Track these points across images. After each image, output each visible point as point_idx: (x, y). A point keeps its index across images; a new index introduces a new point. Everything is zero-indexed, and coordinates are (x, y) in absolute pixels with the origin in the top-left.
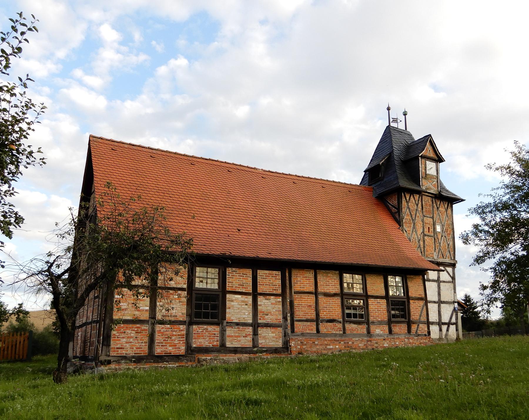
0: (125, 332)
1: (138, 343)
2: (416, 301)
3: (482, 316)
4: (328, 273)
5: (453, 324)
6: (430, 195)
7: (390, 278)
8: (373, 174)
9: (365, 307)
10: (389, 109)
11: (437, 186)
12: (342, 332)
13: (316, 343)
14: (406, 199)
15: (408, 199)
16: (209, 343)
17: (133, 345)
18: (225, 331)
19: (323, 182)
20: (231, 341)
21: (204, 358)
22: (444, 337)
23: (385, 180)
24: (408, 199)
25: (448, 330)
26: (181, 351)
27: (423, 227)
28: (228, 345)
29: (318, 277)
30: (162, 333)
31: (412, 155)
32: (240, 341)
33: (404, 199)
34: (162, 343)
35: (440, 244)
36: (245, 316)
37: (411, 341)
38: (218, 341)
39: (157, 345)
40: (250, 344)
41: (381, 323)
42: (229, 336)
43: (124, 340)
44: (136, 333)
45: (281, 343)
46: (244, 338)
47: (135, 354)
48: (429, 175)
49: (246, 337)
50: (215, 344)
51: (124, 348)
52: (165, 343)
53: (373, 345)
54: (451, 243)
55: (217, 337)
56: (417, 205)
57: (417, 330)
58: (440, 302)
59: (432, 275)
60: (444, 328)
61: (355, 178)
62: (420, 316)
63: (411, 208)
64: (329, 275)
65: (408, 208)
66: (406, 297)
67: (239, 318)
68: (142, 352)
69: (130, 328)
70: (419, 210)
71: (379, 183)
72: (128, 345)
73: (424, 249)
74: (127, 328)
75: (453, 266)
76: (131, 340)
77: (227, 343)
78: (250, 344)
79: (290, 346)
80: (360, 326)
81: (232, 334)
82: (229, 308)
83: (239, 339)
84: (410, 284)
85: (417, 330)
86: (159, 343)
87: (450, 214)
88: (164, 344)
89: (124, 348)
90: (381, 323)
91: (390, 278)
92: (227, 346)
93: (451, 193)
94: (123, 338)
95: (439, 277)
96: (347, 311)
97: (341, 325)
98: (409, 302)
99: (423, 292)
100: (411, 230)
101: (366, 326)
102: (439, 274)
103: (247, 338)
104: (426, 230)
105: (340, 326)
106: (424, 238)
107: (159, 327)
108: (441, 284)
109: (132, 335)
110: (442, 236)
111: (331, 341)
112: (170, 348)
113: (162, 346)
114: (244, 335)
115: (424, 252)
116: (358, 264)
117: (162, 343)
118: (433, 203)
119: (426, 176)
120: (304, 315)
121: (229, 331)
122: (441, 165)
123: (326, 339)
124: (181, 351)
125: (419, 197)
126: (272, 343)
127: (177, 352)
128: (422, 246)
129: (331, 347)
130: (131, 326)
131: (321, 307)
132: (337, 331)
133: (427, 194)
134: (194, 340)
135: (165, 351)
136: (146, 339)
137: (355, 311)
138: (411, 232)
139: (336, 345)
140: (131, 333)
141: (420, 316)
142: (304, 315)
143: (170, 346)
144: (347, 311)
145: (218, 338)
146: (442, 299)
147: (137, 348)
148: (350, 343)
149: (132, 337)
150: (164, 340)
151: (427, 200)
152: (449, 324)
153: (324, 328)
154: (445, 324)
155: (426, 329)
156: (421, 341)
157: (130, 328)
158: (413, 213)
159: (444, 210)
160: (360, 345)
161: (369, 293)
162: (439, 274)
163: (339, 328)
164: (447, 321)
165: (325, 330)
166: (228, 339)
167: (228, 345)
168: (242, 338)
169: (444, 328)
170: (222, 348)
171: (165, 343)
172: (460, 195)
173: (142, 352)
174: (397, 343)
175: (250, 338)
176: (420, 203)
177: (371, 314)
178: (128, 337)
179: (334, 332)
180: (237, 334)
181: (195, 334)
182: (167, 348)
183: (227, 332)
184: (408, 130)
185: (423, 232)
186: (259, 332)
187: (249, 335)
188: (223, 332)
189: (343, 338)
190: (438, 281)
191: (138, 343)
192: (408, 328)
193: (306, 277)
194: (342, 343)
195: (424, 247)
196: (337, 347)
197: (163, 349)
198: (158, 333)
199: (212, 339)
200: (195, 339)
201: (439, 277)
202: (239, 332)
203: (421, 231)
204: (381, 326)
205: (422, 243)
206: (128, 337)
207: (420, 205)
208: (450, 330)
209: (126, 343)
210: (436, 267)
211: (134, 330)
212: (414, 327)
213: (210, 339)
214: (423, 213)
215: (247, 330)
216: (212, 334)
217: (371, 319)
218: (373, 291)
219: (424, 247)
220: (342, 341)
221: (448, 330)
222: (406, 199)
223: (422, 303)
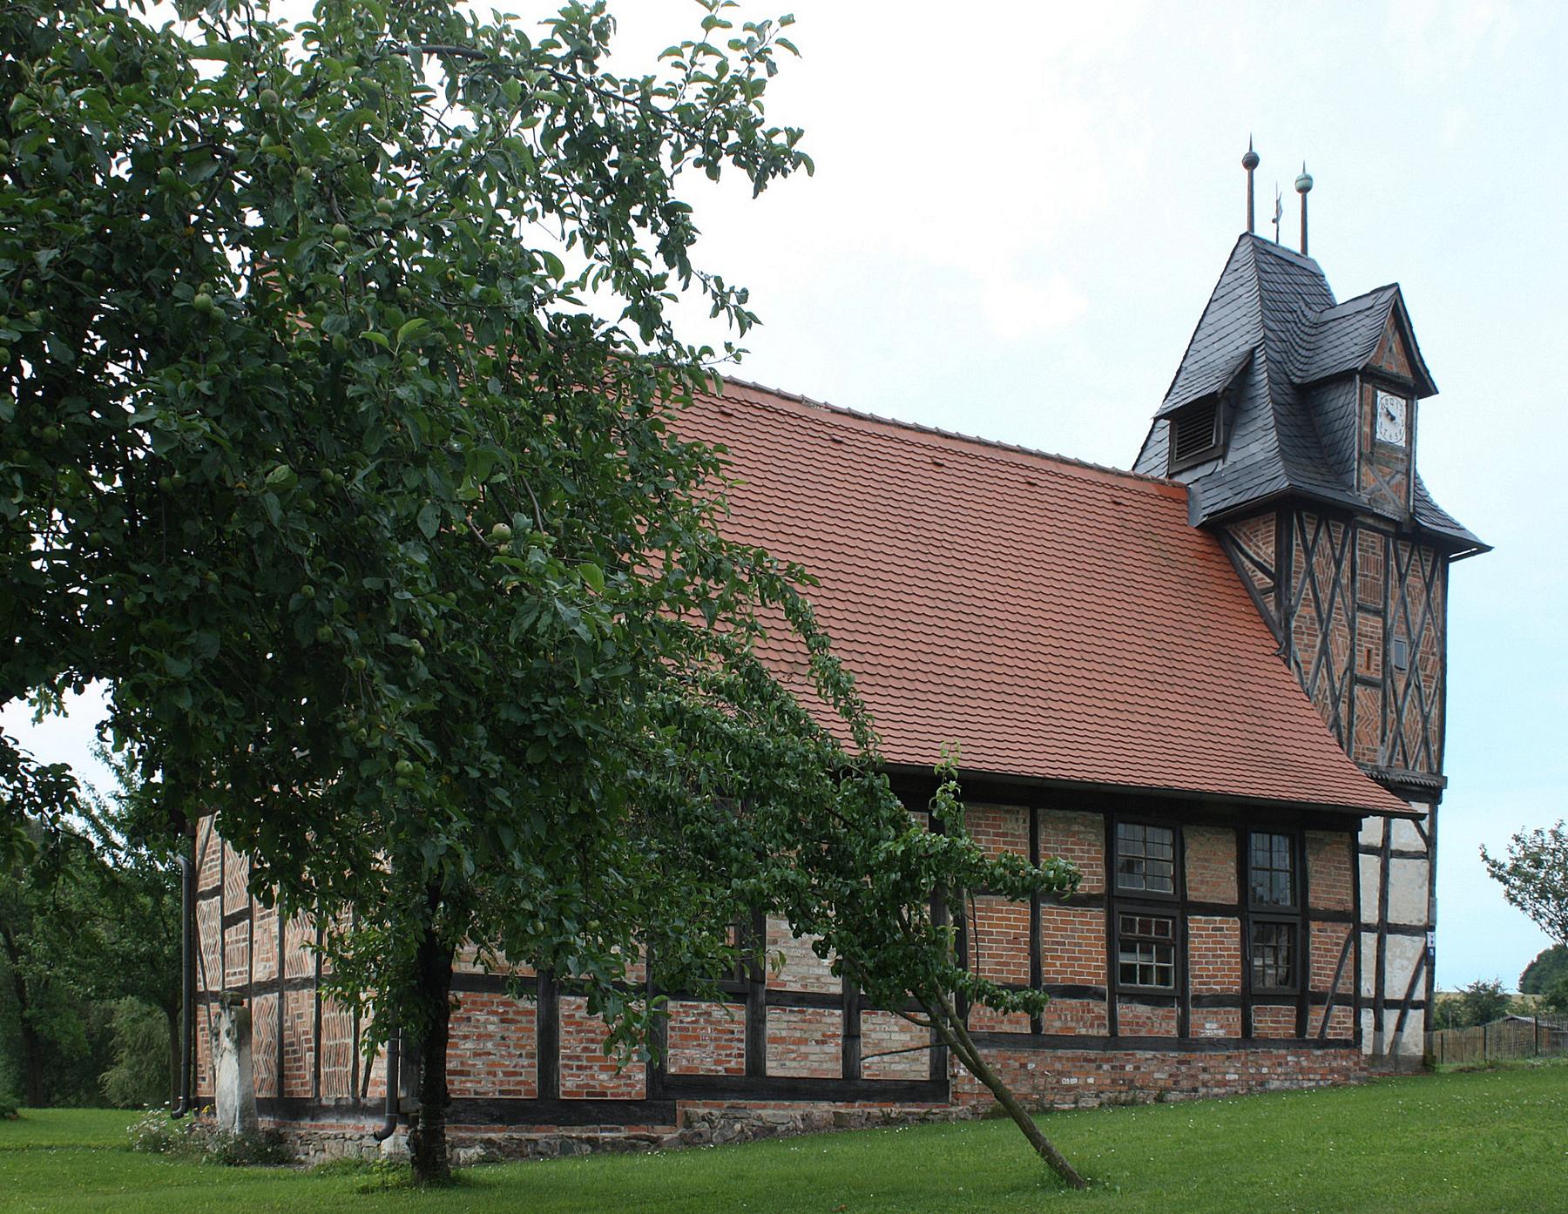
0: (469, 1019)
1: (510, 1055)
2: (1328, 925)
3: (369, 745)
4: (1070, 821)
5: (1417, 1005)
6: (1382, 526)
7: (1258, 841)
8: (1195, 425)
9: (1178, 943)
10: (1251, 162)
11: (1403, 493)
12: (1105, 1032)
13: (1031, 1066)
14: (1304, 540)
15: (1309, 537)
16: (717, 1062)
17: (493, 1064)
18: (763, 1021)
19: (1028, 461)
20: (780, 1058)
21: (702, 1111)
22: (1386, 1051)
23: (1232, 457)
24: (1309, 537)
25: (1400, 1027)
26: (633, 1086)
27: (1352, 650)
28: (773, 1069)
29: (1042, 836)
30: (579, 1024)
31: (1329, 362)
32: (805, 1057)
33: (1296, 541)
34: (578, 1058)
35: (1399, 712)
36: (820, 971)
37: (1305, 1063)
38: (741, 1056)
39: (566, 1066)
40: (834, 1069)
41: (1218, 1001)
42: (775, 1040)
43: (469, 1045)
44: (503, 1021)
45: (926, 1068)
46: (818, 1048)
47: (501, 1092)
48: (1384, 445)
49: (824, 1042)
50: (733, 1064)
51: (467, 1074)
52: (588, 1059)
53: (1194, 1077)
54: (1435, 712)
55: (740, 1041)
56: (1338, 565)
57: (1325, 1023)
58: (1384, 928)
59: (1370, 832)
60: (1391, 1017)
61: (1113, 427)
62: (1337, 977)
63: (1319, 576)
64: (1076, 828)
65: (1310, 573)
66: (1298, 910)
67: (804, 978)
68: (522, 1088)
69: (484, 1004)
70: (1344, 581)
71: (1207, 469)
72: (479, 1063)
73: (1350, 732)
74: (474, 1003)
75: (1433, 794)
76: (490, 1045)
77: (768, 1064)
78: (834, 1069)
79: (955, 1076)
80: (1161, 1012)
81: (784, 1034)
82: (775, 942)
83: (803, 1049)
84: (1313, 865)
85: (1325, 1023)
86: (569, 1058)
87: (1439, 600)
88: (585, 1063)
89: (467, 1074)
90: (1218, 1001)
91: (1258, 841)
92: (770, 1073)
93: (1445, 518)
94: (465, 1037)
95: (1387, 837)
96: (1125, 959)
97: (1105, 1005)
98: (1306, 928)
99: (1350, 892)
100: (1314, 662)
101: (1177, 1010)
102: (1387, 826)
103: (826, 1048)
104: (1360, 660)
105: (1101, 1008)
106: (1351, 691)
107: (569, 1003)
108: (1393, 861)
109: (491, 1028)
110: (1408, 685)
111: (1073, 1059)
112: (604, 1077)
113: (579, 1068)
114: (818, 1036)
115: (1349, 744)
116: (1170, 788)
117: (578, 1058)
118: (1387, 556)
119: (1376, 452)
120: (996, 971)
121: (777, 1022)
122: (1423, 403)
123: (1060, 1052)
124: (633, 1086)
125: (1346, 533)
126: (899, 1067)
127: (624, 1089)
128: (1344, 723)
129: (1074, 1081)
130: (485, 996)
131: (1046, 943)
132: (1092, 1026)
133: (1370, 521)
134: (671, 1052)
135: (588, 1086)
136: (532, 1044)
137: (1145, 957)
138: (1312, 668)
139: (1088, 1075)
140: (487, 1022)
141: (1337, 977)
142: (996, 971)
143: (602, 1069)
144: (1125, 959)
145: (743, 1046)
146: (1392, 918)
147: (505, 1074)
148: (1129, 1068)
149: (490, 1036)
150: (585, 1049)
151: (1370, 545)
152: (1405, 1005)
153: (1059, 1017)
154: (1393, 1004)
155: (1350, 1023)
156: (1334, 1064)
157: (484, 1004)
158: (1324, 596)
159: (1419, 584)
160: (1157, 1075)
161: (1192, 896)
162: (1387, 826)
163: (1097, 1018)
164: (1400, 996)
165: (1058, 1024)
166: (771, 1049)
167: (773, 1069)
168: (812, 1048)
169: (1391, 1017)
170: (754, 1082)
171: (588, 1059)
172: (1476, 528)
173: (522, 1088)
174: (1265, 1070)
175: (834, 1048)
176: (1348, 555)
177: (1194, 970)
178: (480, 1036)
179: (1083, 1031)
180: (798, 1034)
181: (673, 1029)
182: (592, 1077)
183: (768, 1025)
184: (1311, 254)
185: (1351, 667)
186: (864, 1027)
187: (834, 1036)
188: (756, 1026)
189: (1110, 1054)
190: (1384, 851)
191: (510, 1055)
192: (1298, 1017)
193: (1005, 835)
194: (1105, 1067)
195: (1350, 724)
196: (1091, 1081)
197: (582, 1080)
198: (567, 1024)
199: (723, 1048)
200: (674, 1046)
201: (1387, 837)
202: (805, 1026)
203: (1344, 665)
204: (1222, 1010)
205: (1343, 708)
206: (480, 1036)
207: (1345, 565)
208: (1407, 1030)
209: (476, 1055)
210: (1395, 803)
211: (495, 1013)
212: (1316, 1016)
213: (717, 1047)
214: (1353, 594)
215: (828, 1020)
216: (723, 1031)
217: (1194, 986)
218: (1203, 888)
219: (1350, 724)
220: (1108, 1061)
221: (1400, 1027)
222: (1304, 540)
223: (1342, 931)
